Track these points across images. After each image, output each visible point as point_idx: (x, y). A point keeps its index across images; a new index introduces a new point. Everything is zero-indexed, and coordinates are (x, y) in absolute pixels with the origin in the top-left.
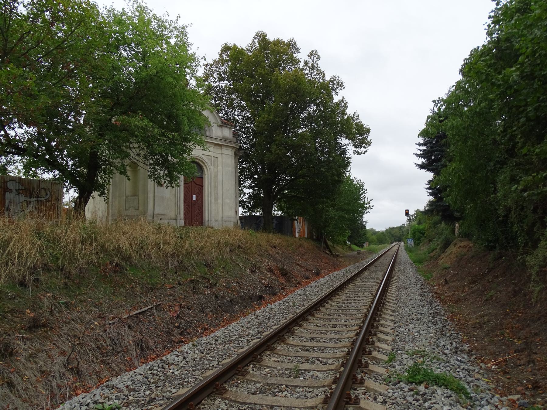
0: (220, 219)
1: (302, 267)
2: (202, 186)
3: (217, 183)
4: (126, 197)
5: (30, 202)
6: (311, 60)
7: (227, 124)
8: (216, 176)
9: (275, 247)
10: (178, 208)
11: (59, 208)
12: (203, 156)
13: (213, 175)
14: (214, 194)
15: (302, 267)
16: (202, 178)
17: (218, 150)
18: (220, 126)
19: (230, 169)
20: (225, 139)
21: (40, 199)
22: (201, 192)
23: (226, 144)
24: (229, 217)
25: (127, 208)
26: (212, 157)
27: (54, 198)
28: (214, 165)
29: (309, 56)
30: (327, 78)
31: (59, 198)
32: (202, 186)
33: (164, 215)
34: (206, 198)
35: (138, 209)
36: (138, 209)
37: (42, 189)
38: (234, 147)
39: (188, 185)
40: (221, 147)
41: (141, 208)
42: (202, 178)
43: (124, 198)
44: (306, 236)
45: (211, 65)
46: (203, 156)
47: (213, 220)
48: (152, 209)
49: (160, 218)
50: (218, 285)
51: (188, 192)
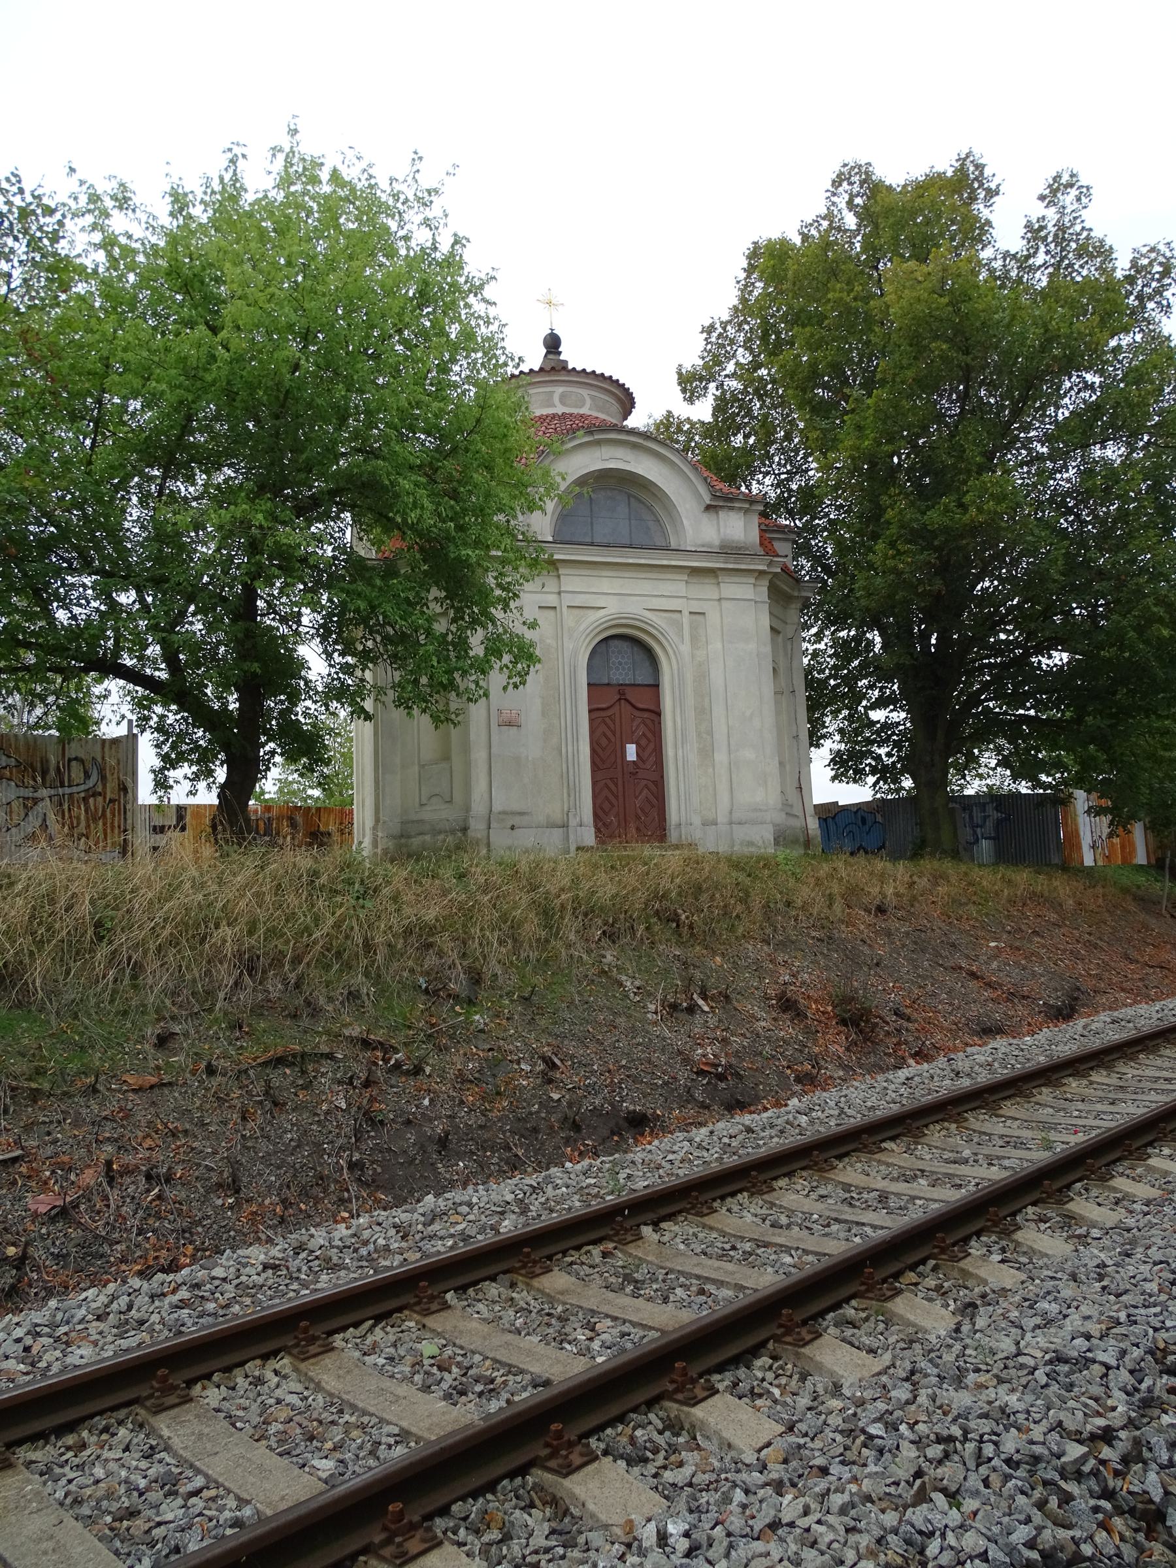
0: (722, 818)
1: (989, 985)
2: (659, 714)
3: (707, 700)
4: (422, 766)
5: (36, 801)
6: (1052, 214)
7: (731, 500)
8: (702, 677)
9: (881, 910)
10: (572, 790)
11: (129, 814)
12: (648, 614)
13: (689, 676)
14: (699, 735)
15: (989, 985)
16: (656, 686)
17: (706, 590)
18: (708, 508)
19: (752, 646)
20: (729, 550)
21: (67, 790)
22: (654, 734)
23: (731, 566)
24: (755, 810)
25: (424, 801)
26: (686, 613)
27: (111, 785)
28: (694, 639)
29: (1042, 198)
30: (1122, 265)
31: (129, 785)
32: (657, 713)
33: (522, 814)
34: (669, 751)
35: (450, 802)
36: (450, 802)
37: (70, 760)
38: (761, 573)
39: (609, 713)
40: (717, 577)
41: (458, 797)
42: (658, 686)
43: (416, 768)
44: (1141, 858)
45: (724, 325)
46: (648, 614)
47: (697, 820)
48: (486, 796)
49: (509, 824)
50: (428, 1070)
51: (609, 734)
